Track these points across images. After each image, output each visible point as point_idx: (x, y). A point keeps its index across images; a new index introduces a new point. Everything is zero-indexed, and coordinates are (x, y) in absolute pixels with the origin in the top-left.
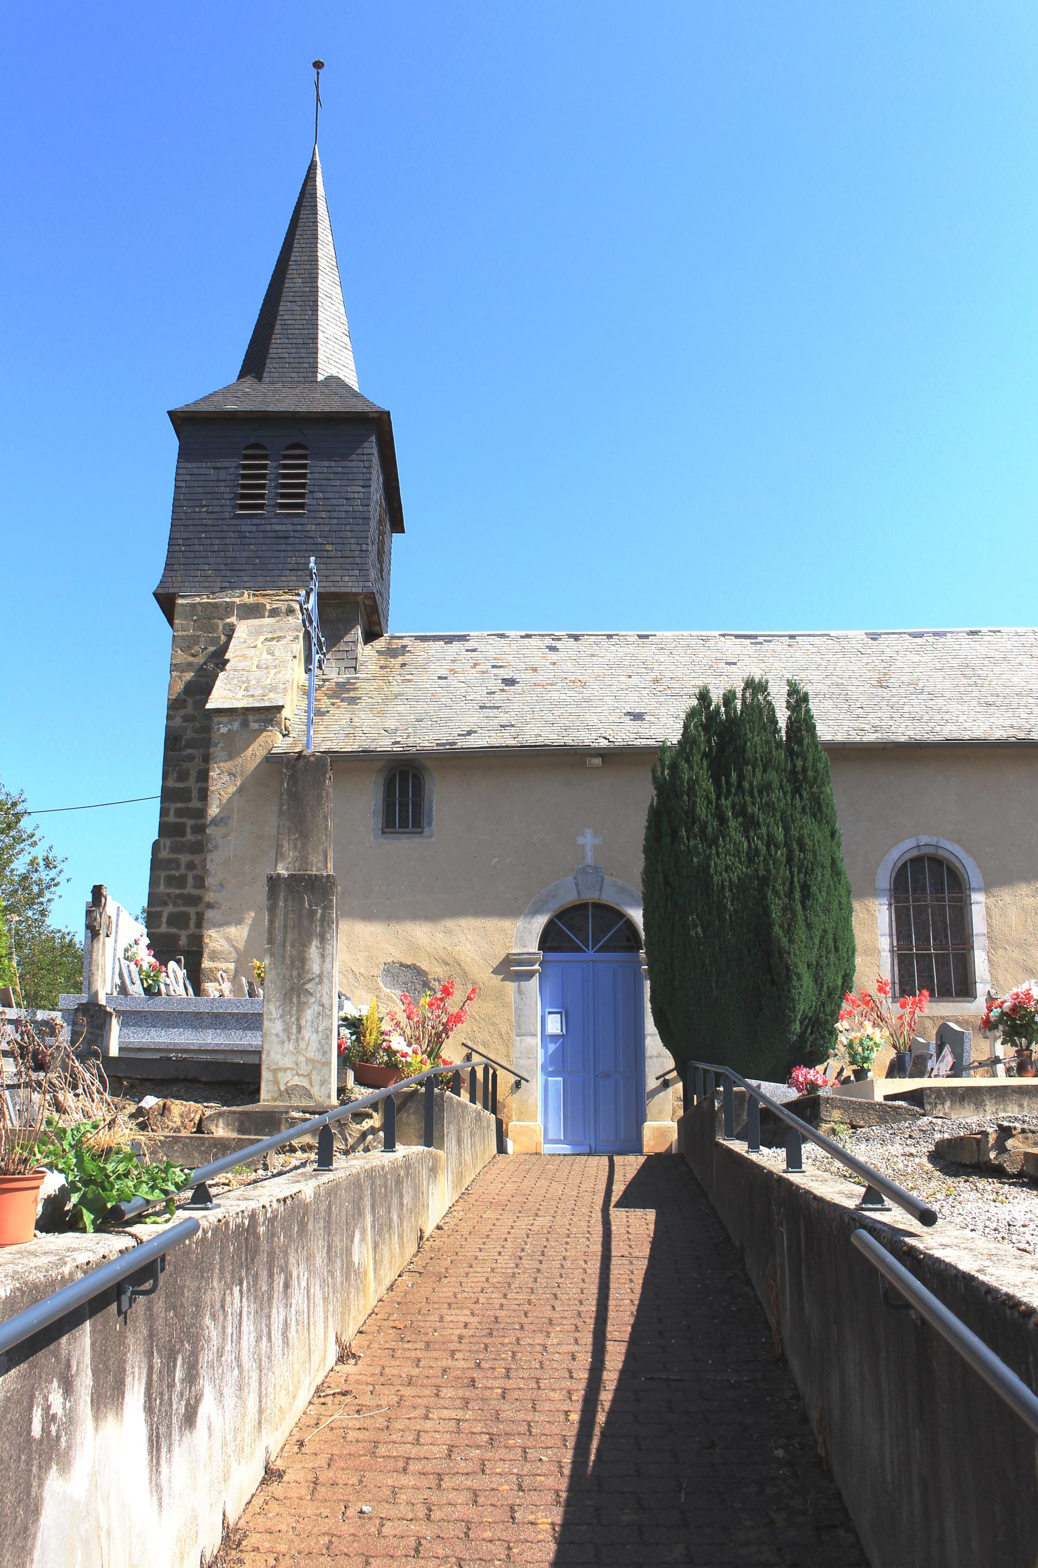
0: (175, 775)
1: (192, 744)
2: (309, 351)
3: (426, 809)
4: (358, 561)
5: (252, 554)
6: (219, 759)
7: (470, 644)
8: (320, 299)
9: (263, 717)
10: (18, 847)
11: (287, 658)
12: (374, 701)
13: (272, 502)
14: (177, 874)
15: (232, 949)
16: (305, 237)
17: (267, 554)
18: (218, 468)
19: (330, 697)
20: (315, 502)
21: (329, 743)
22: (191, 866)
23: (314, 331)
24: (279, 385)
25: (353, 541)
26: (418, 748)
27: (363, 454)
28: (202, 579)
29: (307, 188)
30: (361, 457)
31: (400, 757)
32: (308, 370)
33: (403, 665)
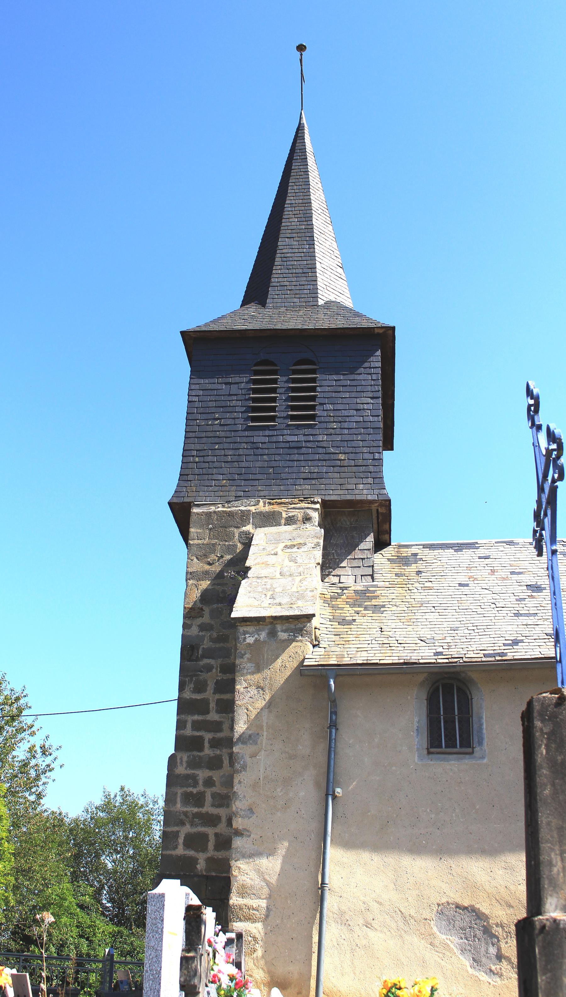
0: (192, 686)
1: (209, 654)
2: (309, 279)
3: (475, 726)
4: (371, 469)
5: (266, 464)
6: (245, 671)
7: (482, 552)
8: (315, 235)
9: (292, 626)
10: (19, 736)
11: (311, 565)
12: (399, 609)
13: (284, 414)
14: (195, 791)
15: (264, 884)
16: (298, 184)
17: (281, 464)
18: (230, 384)
19: (353, 605)
20: (325, 414)
21: (364, 654)
22: (209, 782)
23: (312, 262)
24: (283, 309)
25: (365, 450)
26: (465, 660)
27: (370, 368)
28: (216, 489)
29: (297, 145)
30: (368, 371)
31: (447, 670)
32: (309, 295)
33: (419, 573)
